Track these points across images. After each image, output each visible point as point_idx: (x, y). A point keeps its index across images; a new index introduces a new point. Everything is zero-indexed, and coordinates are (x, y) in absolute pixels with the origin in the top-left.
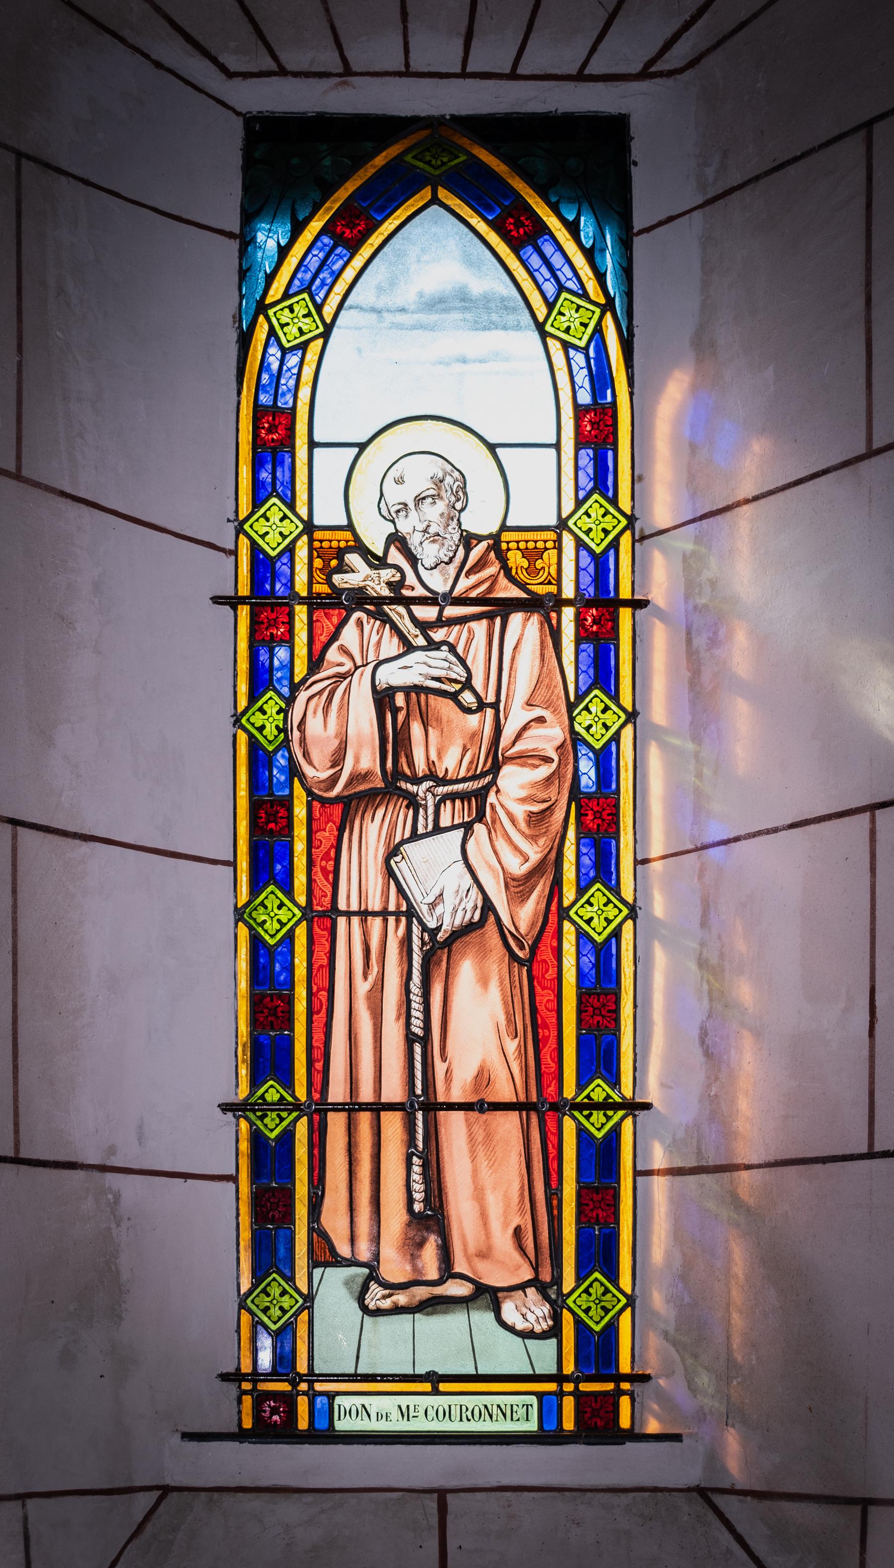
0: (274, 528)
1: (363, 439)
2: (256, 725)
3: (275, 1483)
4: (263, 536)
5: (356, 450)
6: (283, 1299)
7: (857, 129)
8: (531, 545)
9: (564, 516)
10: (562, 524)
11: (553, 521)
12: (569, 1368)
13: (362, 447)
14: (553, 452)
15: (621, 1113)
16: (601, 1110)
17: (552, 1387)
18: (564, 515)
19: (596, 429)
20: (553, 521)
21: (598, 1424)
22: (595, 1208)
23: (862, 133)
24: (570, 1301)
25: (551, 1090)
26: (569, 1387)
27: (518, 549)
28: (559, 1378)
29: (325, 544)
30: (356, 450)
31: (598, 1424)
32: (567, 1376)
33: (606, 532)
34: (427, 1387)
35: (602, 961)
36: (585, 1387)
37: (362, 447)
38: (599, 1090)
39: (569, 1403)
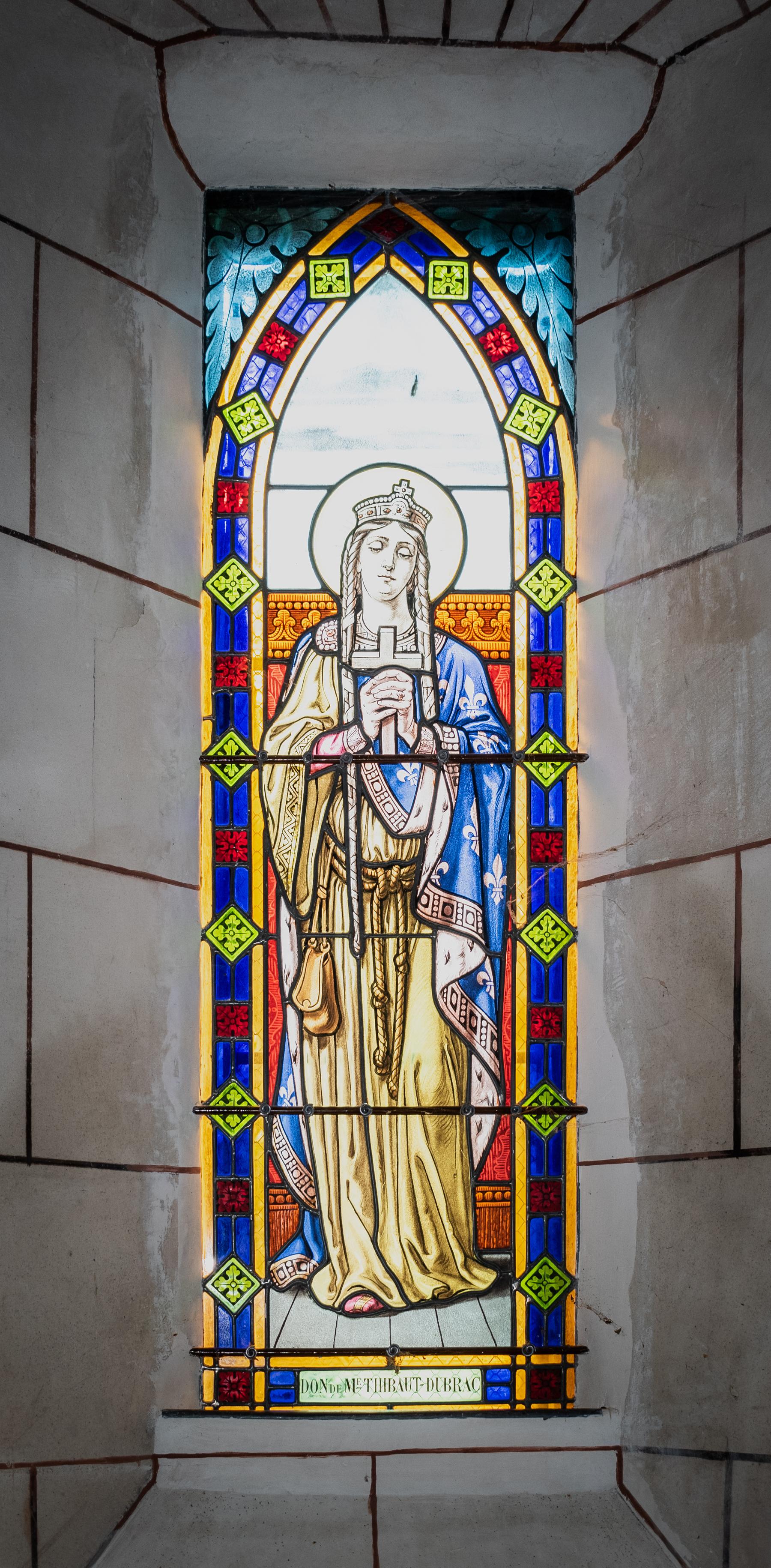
0: (236, 585)
1: (333, 482)
2: (220, 589)
3: (273, 185)
4: (222, 593)
5: (324, 492)
6: (225, 1287)
7: (730, 250)
8: (488, 606)
9: (517, 578)
10: (515, 585)
11: (507, 586)
12: (521, 1341)
13: (330, 489)
14: (506, 493)
15: (567, 764)
16: (550, 761)
17: (505, 1360)
18: (517, 578)
19: (545, 499)
20: (507, 586)
21: (549, 1389)
22: (544, 1021)
23: (736, 254)
24: (523, 935)
25: (503, 1125)
26: (521, 1360)
27: (318, 609)
28: (513, 1351)
29: (297, 606)
30: (325, 492)
31: (549, 1389)
32: (520, 1349)
33: (554, 592)
34: (381, 1361)
35: (550, 981)
36: (535, 1360)
37: (330, 489)
38: (548, 744)
39: (521, 1377)
